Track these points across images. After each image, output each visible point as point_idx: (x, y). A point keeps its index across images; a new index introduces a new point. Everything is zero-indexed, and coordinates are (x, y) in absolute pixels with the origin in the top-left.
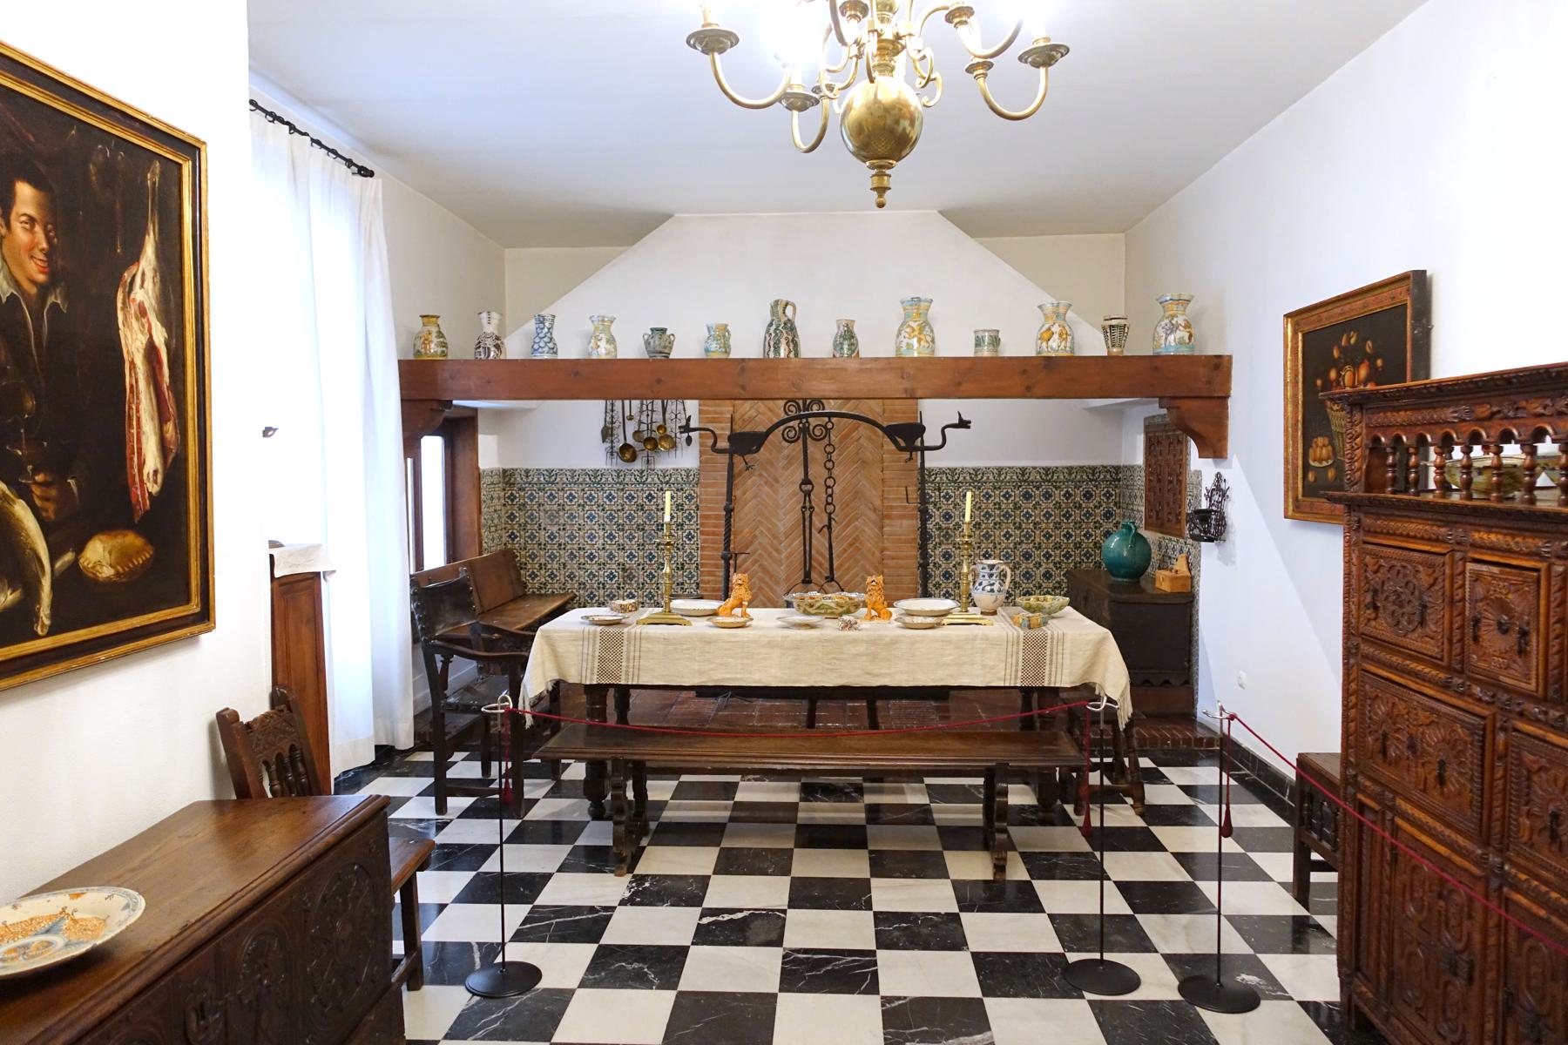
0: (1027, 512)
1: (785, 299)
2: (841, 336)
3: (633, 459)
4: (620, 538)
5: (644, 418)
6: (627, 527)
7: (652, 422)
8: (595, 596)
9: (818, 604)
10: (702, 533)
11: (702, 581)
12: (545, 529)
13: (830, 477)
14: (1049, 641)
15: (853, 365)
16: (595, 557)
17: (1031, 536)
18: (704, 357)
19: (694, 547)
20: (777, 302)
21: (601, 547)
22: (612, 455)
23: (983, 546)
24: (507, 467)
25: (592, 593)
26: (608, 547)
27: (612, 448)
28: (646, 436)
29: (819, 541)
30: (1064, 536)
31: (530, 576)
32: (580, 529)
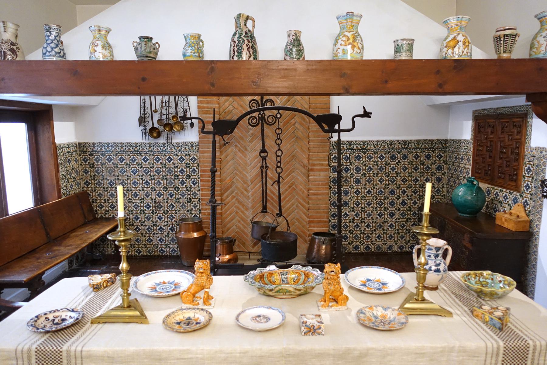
0: (393, 167)
1: (247, 13)
2: (291, 44)
3: (159, 136)
4: (152, 184)
5: (164, 111)
6: (156, 178)
7: (169, 114)
8: (139, 218)
9: (277, 289)
10: (201, 181)
11: (202, 209)
12: (106, 179)
13: (279, 150)
14: (531, 352)
15: (301, 67)
16: (138, 195)
17: (395, 181)
18: (183, 59)
19: (197, 189)
20: (239, 16)
21: (141, 189)
22: (145, 134)
23: (367, 186)
24: (81, 141)
25: (137, 216)
26: (145, 189)
27: (145, 129)
28: (165, 122)
29: (272, 189)
30: (414, 180)
31: (99, 206)
32: (128, 179)
